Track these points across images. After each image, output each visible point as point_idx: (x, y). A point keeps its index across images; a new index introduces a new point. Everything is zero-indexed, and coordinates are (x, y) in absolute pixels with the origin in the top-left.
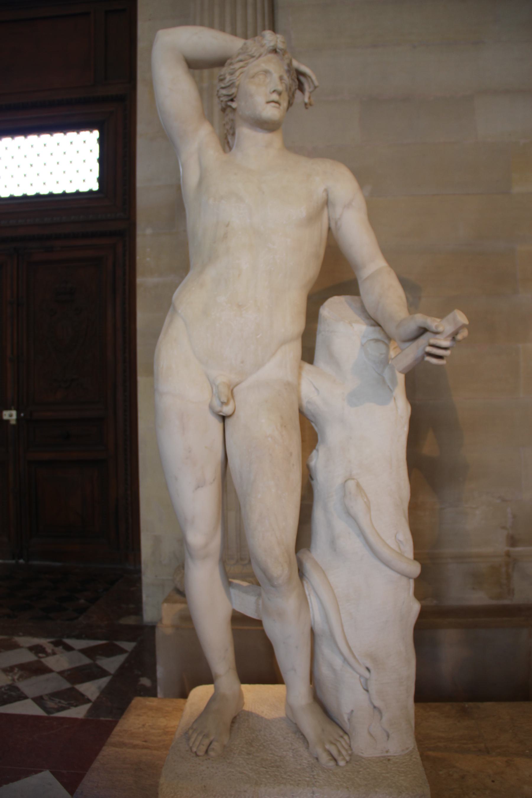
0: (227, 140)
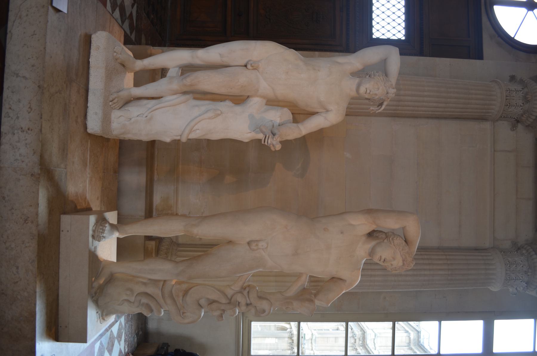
0: (355, 74)
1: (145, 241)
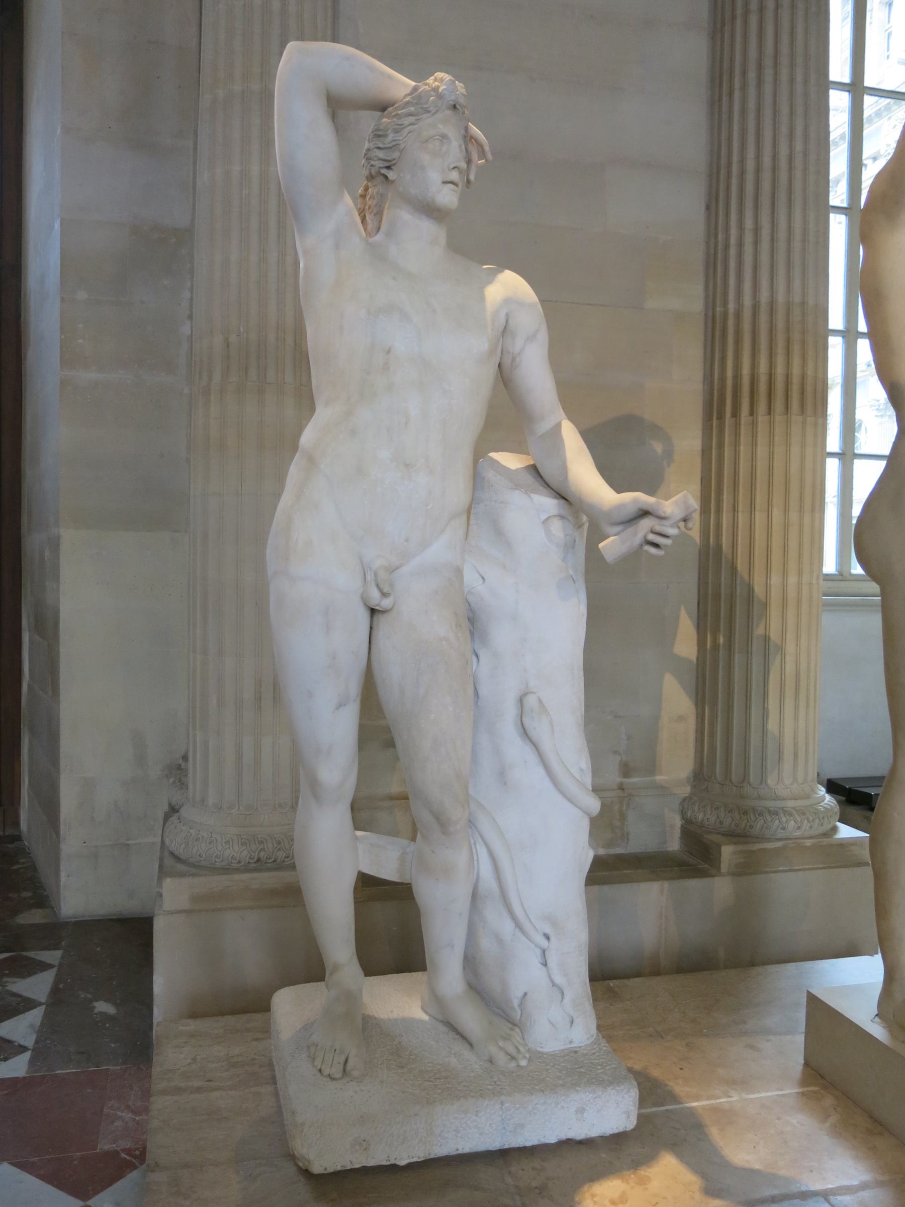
1: (723, 875)
